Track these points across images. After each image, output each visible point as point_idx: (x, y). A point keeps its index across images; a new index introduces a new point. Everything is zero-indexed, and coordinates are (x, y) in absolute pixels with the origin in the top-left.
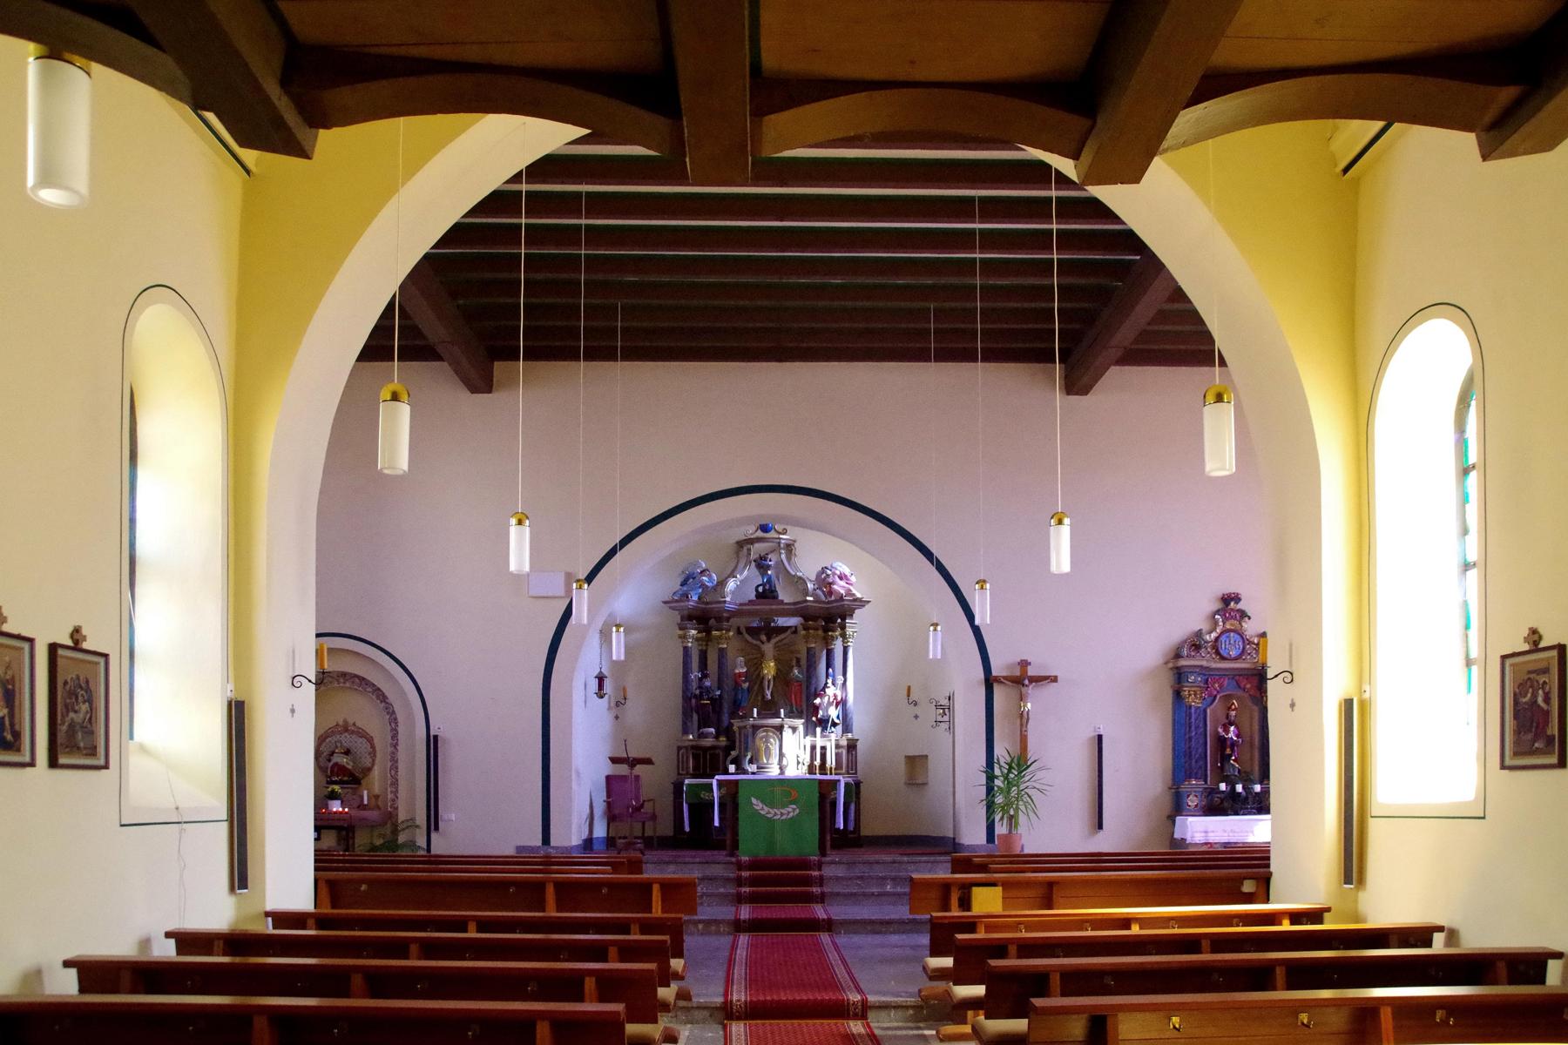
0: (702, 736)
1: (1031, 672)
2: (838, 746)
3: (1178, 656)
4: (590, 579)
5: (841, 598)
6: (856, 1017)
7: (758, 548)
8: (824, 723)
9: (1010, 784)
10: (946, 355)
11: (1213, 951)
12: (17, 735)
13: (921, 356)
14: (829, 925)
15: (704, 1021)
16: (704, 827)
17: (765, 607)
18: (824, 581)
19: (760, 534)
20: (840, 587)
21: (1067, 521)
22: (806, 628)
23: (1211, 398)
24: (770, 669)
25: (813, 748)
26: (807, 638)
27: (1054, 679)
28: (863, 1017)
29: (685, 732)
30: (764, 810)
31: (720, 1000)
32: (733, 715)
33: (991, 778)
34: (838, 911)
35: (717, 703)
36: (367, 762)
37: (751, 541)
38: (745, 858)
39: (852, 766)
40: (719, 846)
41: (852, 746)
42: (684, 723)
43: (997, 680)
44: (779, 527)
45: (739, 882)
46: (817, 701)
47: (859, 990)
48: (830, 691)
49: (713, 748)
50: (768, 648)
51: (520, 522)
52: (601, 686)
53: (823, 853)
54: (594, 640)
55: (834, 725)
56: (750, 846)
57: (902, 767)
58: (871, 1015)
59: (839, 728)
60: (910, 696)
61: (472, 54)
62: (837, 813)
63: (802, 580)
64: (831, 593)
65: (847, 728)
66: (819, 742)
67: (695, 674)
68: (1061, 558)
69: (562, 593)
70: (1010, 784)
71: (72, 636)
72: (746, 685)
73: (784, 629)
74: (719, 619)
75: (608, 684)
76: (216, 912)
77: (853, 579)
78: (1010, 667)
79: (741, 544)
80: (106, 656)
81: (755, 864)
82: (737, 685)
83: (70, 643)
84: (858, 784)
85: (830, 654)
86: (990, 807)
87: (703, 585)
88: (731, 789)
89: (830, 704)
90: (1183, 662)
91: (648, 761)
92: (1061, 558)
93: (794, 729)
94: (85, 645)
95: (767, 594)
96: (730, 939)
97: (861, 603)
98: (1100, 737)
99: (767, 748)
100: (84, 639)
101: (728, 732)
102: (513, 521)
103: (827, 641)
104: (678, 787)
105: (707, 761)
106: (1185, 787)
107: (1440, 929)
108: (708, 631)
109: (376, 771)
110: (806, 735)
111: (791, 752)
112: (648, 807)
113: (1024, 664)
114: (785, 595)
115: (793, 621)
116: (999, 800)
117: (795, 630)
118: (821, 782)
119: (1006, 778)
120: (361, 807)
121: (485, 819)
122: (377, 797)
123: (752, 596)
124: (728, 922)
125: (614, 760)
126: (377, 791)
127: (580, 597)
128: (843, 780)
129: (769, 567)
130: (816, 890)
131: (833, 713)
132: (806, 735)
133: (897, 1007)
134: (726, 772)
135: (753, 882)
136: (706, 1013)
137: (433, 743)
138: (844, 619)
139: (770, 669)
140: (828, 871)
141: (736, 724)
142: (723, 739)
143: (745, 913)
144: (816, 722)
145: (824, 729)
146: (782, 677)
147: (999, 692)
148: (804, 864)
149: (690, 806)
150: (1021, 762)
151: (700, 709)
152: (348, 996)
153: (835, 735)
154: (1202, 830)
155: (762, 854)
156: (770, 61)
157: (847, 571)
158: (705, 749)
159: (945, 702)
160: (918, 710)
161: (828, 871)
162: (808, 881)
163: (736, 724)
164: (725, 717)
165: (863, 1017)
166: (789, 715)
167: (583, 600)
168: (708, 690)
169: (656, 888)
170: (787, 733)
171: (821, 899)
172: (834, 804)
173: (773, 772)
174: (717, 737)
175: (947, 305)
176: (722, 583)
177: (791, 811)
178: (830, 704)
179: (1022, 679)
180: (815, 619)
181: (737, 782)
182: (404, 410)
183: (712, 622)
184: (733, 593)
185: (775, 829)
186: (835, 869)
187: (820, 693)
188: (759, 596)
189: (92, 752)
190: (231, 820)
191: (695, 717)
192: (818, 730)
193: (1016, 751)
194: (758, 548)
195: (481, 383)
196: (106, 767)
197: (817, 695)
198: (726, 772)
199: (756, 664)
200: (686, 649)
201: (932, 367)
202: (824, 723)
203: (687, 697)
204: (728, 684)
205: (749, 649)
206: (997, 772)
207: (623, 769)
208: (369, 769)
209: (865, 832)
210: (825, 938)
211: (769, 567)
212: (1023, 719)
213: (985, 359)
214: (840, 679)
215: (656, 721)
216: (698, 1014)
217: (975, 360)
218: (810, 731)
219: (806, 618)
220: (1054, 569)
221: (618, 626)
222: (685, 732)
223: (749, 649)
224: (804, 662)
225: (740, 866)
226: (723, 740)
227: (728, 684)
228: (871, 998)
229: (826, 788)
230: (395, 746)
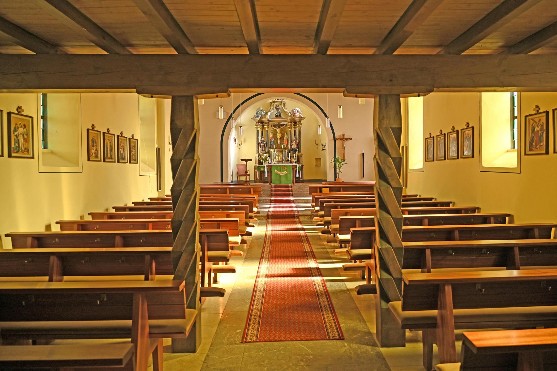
1: (345, 137)
11: (409, 214)
17: (278, 119)
24: (279, 136)
28: (298, 218)
30: (278, 173)
37: (274, 102)
43: (337, 139)
56: (275, 182)
58: (300, 217)
67: (260, 137)
71: (17, 110)
73: (283, 125)
76: (155, 195)
78: (340, 136)
79: (271, 103)
80: (32, 118)
81: (275, 187)
83: (17, 112)
91: (251, 160)
94: (95, 129)
95: (278, 116)
100: (23, 111)
107: (451, 202)
123: (275, 116)
130: (291, 193)
148: (288, 187)
152: (114, 246)
157: (299, 110)
162: (288, 191)
165: (298, 218)
177: (285, 173)
179: (343, 138)
188: (277, 117)
189: (135, 160)
190: (157, 175)
196: (33, 158)
203: (258, 143)
212: (343, 149)
216: (262, 218)
224: (289, 134)
225: (271, 187)
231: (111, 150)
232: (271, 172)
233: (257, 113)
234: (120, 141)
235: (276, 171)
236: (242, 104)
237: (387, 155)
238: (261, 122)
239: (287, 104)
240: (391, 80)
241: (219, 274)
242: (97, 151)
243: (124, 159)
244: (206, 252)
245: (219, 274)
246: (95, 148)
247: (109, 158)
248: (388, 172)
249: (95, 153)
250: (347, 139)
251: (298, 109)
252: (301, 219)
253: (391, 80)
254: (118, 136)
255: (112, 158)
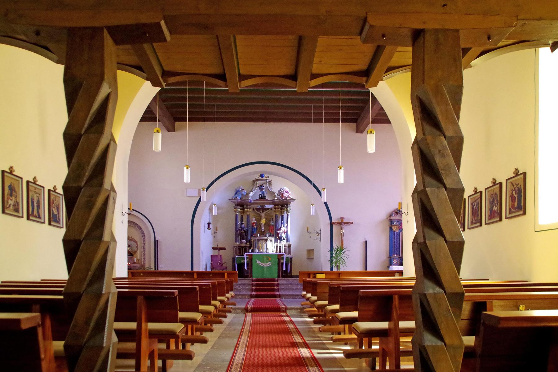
0: (241, 243)
1: (345, 221)
2: (285, 246)
3: (391, 216)
4: (207, 189)
5: (286, 198)
6: (283, 312)
7: (259, 183)
8: (280, 239)
9: (337, 256)
10: (327, 121)
12: (59, 219)
13: (309, 120)
14: (279, 296)
15: (240, 313)
16: (243, 272)
17: (262, 201)
18: (281, 193)
19: (260, 178)
20: (286, 195)
21: (343, 168)
22: (275, 208)
23: (369, 132)
24: (263, 222)
25: (277, 247)
26: (275, 211)
27: (352, 223)
28: (285, 312)
29: (236, 241)
30: (261, 264)
31: (244, 307)
32: (252, 236)
33: (332, 254)
34: (282, 293)
35: (246, 232)
36: (135, 249)
38: (254, 278)
39: (290, 253)
40: (247, 277)
41: (289, 246)
42: (236, 239)
43: (334, 223)
44: (266, 176)
45: (253, 285)
46: (278, 232)
47: (284, 305)
48: (283, 228)
49: (245, 247)
50: (263, 215)
51: (187, 168)
52: (209, 226)
53: (279, 277)
54: (207, 212)
55: (284, 239)
56: (256, 275)
57: (305, 253)
58: (288, 311)
59: (285, 241)
60: (310, 231)
61: (192, 72)
62: (284, 266)
63: (273, 193)
64: (283, 197)
65: (288, 241)
66: (279, 245)
67: (239, 223)
68: (341, 179)
69: (197, 195)
70: (337, 256)
72: (256, 227)
73: (268, 209)
74: (247, 205)
75: (211, 225)
77: (290, 192)
78: (338, 219)
79: (255, 181)
81: (257, 280)
82: (253, 226)
84: (291, 258)
85: (283, 216)
86: (331, 262)
87: (242, 194)
88: (251, 258)
89: (282, 232)
90: (392, 218)
91: (224, 249)
92: (341, 179)
93: (271, 241)
95: (262, 197)
96: (248, 300)
97: (292, 200)
98: (366, 241)
99: (262, 247)
101: (250, 241)
102: (185, 168)
103: (282, 212)
104: (234, 259)
105: (242, 250)
106: (392, 257)
108: (244, 209)
109: (138, 251)
110: (275, 242)
111: (271, 247)
112: (224, 265)
113: (342, 218)
114: (268, 198)
115: (271, 206)
116: (334, 261)
117: (272, 209)
118: (278, 255)
119: (336, 252)
120: (134, 263)
121: (174, 260)
122: (138, 260)
123: (258, 198)
124: (248, 295)
125: (214, 248)
126: (138, 258)
127: (203, 194)
128: (285, 256)
129: (263, 189)
130: (276, 288)
131: (284, 235)
132: (275, 242)
133: (295, 309)
134: (249, 252)
135: (257, 285)
136: (240, 310)
137: (156, 243)
138: (287, 205)
139: (263, 222)
140: (280, 282)
141: (253, 239)
142: (248, 244)
143: (254, 293)
144: (278, 238)
145: (281, 240)
146: (267, 224)
147: (334, 227)
148: (273, 280)
149: (238, 265)
150: (341, 249)
151: (241, 234)
153: (284, 242)
154: (395, 268)
155: (260, 278)
156: (242, 72)
157: (288, 190)
158: (242, 247)
159: (319, 232)
160: (311, 235)
161: (280, 282)
162: (274, 285)
163: (253, 239)
164: (249, 238)
165: (285, 312)
166: (270, 236)
167: (204, 195)
168: (243, 228)
169: (226, 274)
170: (269, 242)
171: (278, 290)
172: (283, 264)
173: (265, 252)
174: (246, 243)
175: (317, 105)
176: (248, 194)
177: (269, 264)
178: (282, 232)
179: (342, 223)
180: (278, 205)
181: (252, 255)
182: (160, 135)
183: (245, 206)
184: (252, 197)
185: (264, 269)
186: (282, 282)
187: (280, 229)
188: (260, 198)
191: (239, 237)
192: (279, 241)
193: (339, 246)
194: (259, 183)
195: (171, 129)
197: (278, 230)
198: (249, 252)
199: (259, 220)
200: (236, 215)
201: (323, 125)
202: (280, 239)
203: (236, 231)
204: (250, 225)
205: (256, 214)
206: (334, 252)
207: (216, 252)
208: (136, 252)
209: (293, 274)
210: (278, 299)
211: (263, 189)
212: (342, 235)
213: (325, 122)
214: (286, 225)
215: (227, 237)
217: (322, 122)
218: (276, 241)
219: (275, 205)
220: (339, 182)
221: (215, 204)
222: (236, 241)
223: (256, 214)
224: (274, 220)
225: (253, 281)
226: (248, 244)
227: (250, 225)
228: (288, 307)
229: (280, 257)
230: (144, 244)
231: (38, 207)
232: (252, 265)
233: (236, 194)
234: (52, 197)
235: (258, 262)
236: (217, 179)
237: (438, 133)
238: (242, 205)
239: (273, 183)
240: (444, 5)
241: (169, 362)
242: (18, 203)
243: (58, 222)
244: (143, 325)
245: (169, 362)
246: (13, 198)
247: (35, 217)
248: (440, 162)
249: (14, 205)
250: (346, 223)
251: (286, 189)
252: (288, 312)
253: (444, 5)
254: (49, 191)
255: (40, 218)
